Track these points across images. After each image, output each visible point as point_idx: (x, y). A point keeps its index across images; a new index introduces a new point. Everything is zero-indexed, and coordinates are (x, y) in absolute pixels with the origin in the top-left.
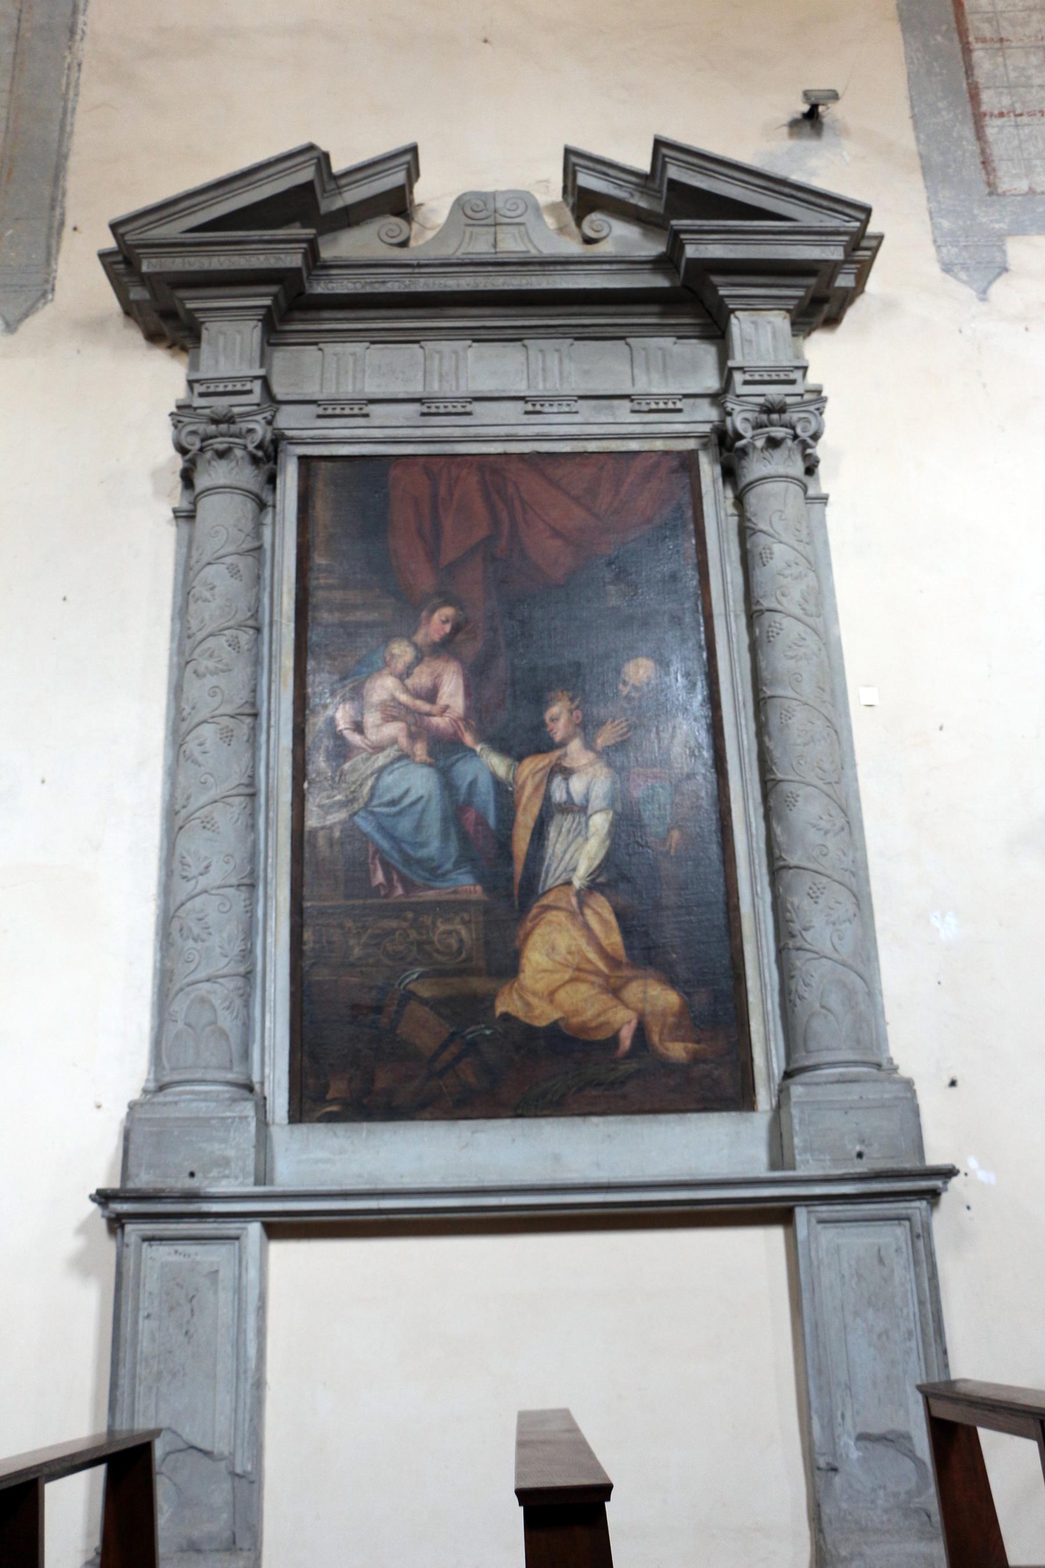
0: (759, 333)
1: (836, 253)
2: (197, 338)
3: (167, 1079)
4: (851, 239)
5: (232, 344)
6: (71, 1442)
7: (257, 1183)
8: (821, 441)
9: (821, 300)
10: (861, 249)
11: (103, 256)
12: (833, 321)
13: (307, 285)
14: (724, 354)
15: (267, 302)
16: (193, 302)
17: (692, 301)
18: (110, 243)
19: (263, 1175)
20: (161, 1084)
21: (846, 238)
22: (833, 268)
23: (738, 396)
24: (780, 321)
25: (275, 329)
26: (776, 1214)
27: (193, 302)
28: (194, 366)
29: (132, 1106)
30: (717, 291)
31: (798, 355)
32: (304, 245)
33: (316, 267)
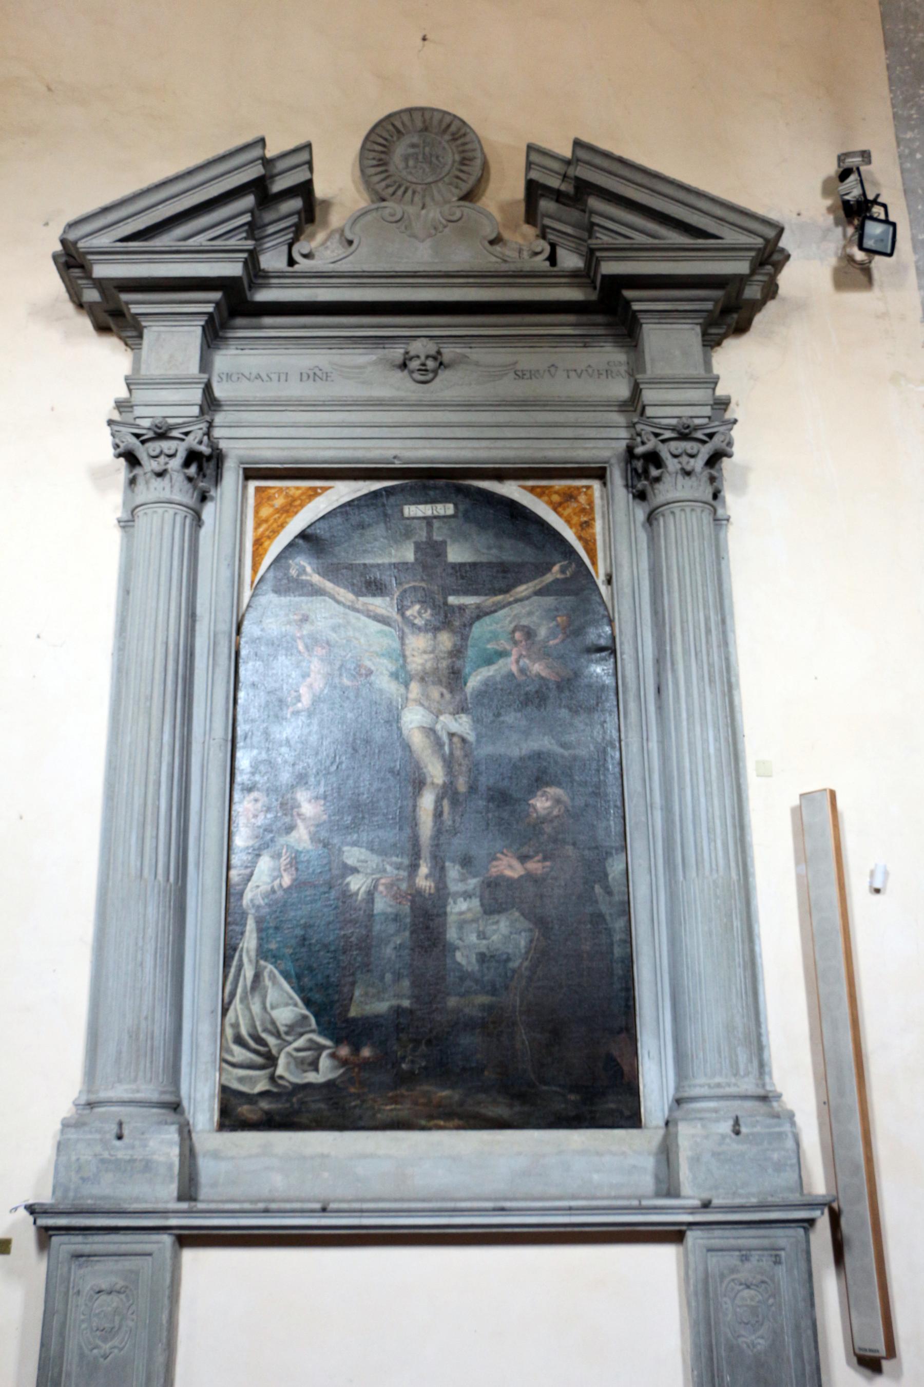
0: (669, 342)
1: (741, 267)
2: (141, 336)
3: (103, 1095)
4: (757, 255)
5: (175, 343)
6: (682, 1324)
7: (180, 1199)
8: (885, 66)
9: (731, 310)
10: (770, 258)
11: (55, 257)
12: (742, 328)
13: (248, 294)
14: (636, 366)
15: (210, 308)
16: (136, 304)
17: (612, 309)
18: (59, 247)
19: (188, 1189)
20: (93, 1098)
21: (753, 254)
22: (741, 280)
23: (649, 418)
24: (689, 335)
25: (214, 334)
26: (673, 1235)
27: (136, 304)
28: (137, 363)
29: (66, 1125)
30: (630, 307)
31: (708, 365)
32: (245, 255)
33: (256, 276)
